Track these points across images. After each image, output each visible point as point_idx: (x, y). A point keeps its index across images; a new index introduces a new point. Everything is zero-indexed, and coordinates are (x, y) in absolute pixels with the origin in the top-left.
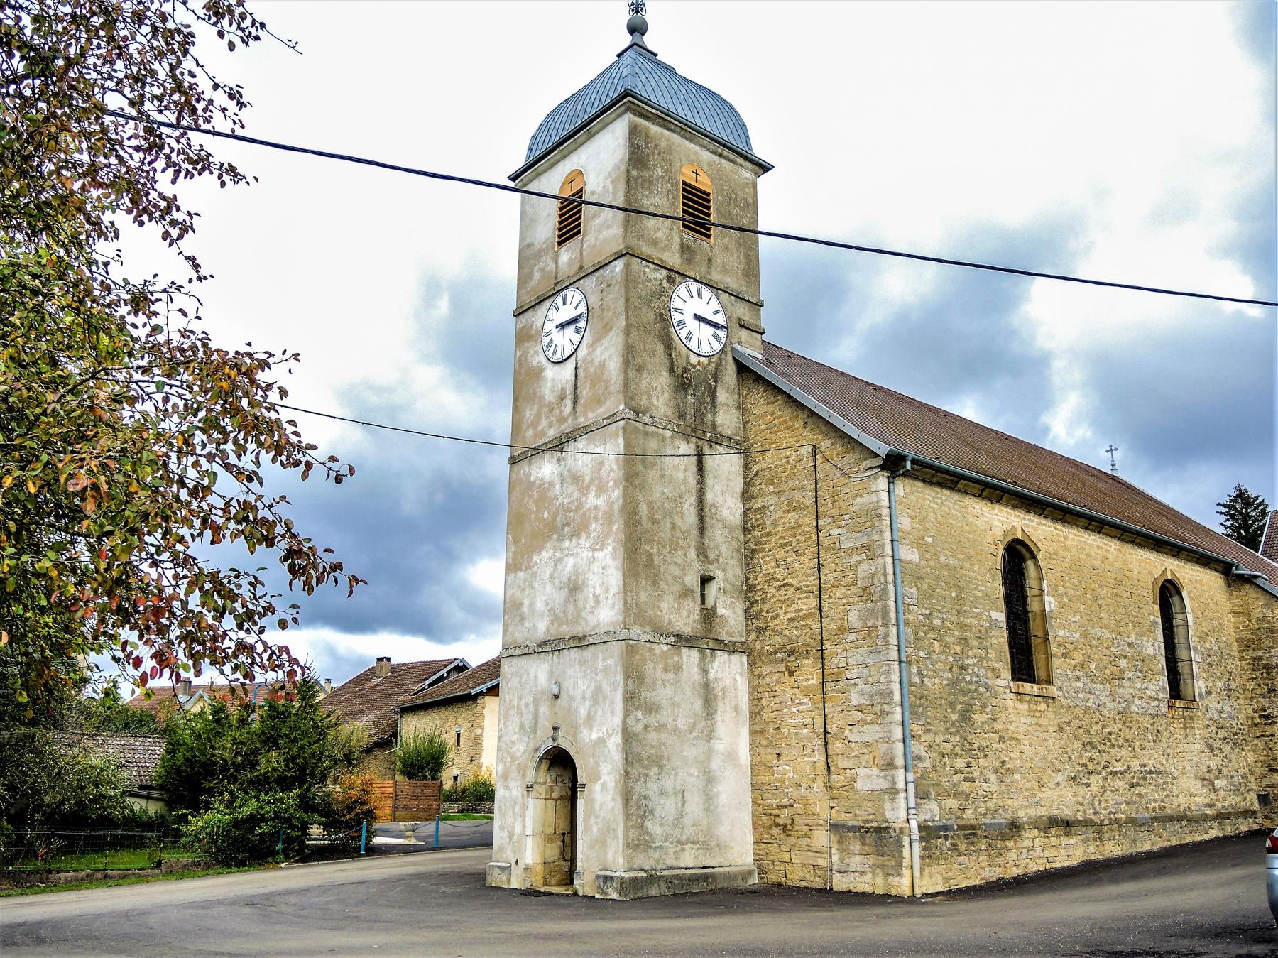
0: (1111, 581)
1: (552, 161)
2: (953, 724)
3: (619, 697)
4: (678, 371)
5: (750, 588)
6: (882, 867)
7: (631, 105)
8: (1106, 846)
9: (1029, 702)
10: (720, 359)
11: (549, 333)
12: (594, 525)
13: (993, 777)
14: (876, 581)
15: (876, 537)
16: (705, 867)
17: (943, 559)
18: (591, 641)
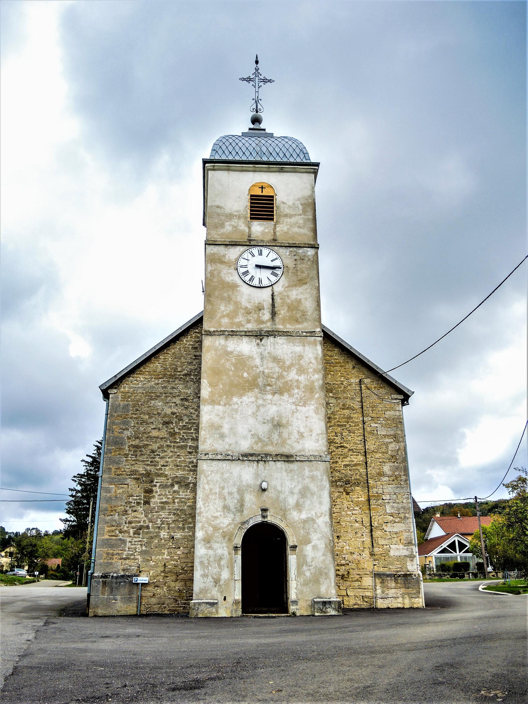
1: (244, 168)
6: (408, 594)
14: (399, 453)
18: (298, 459)
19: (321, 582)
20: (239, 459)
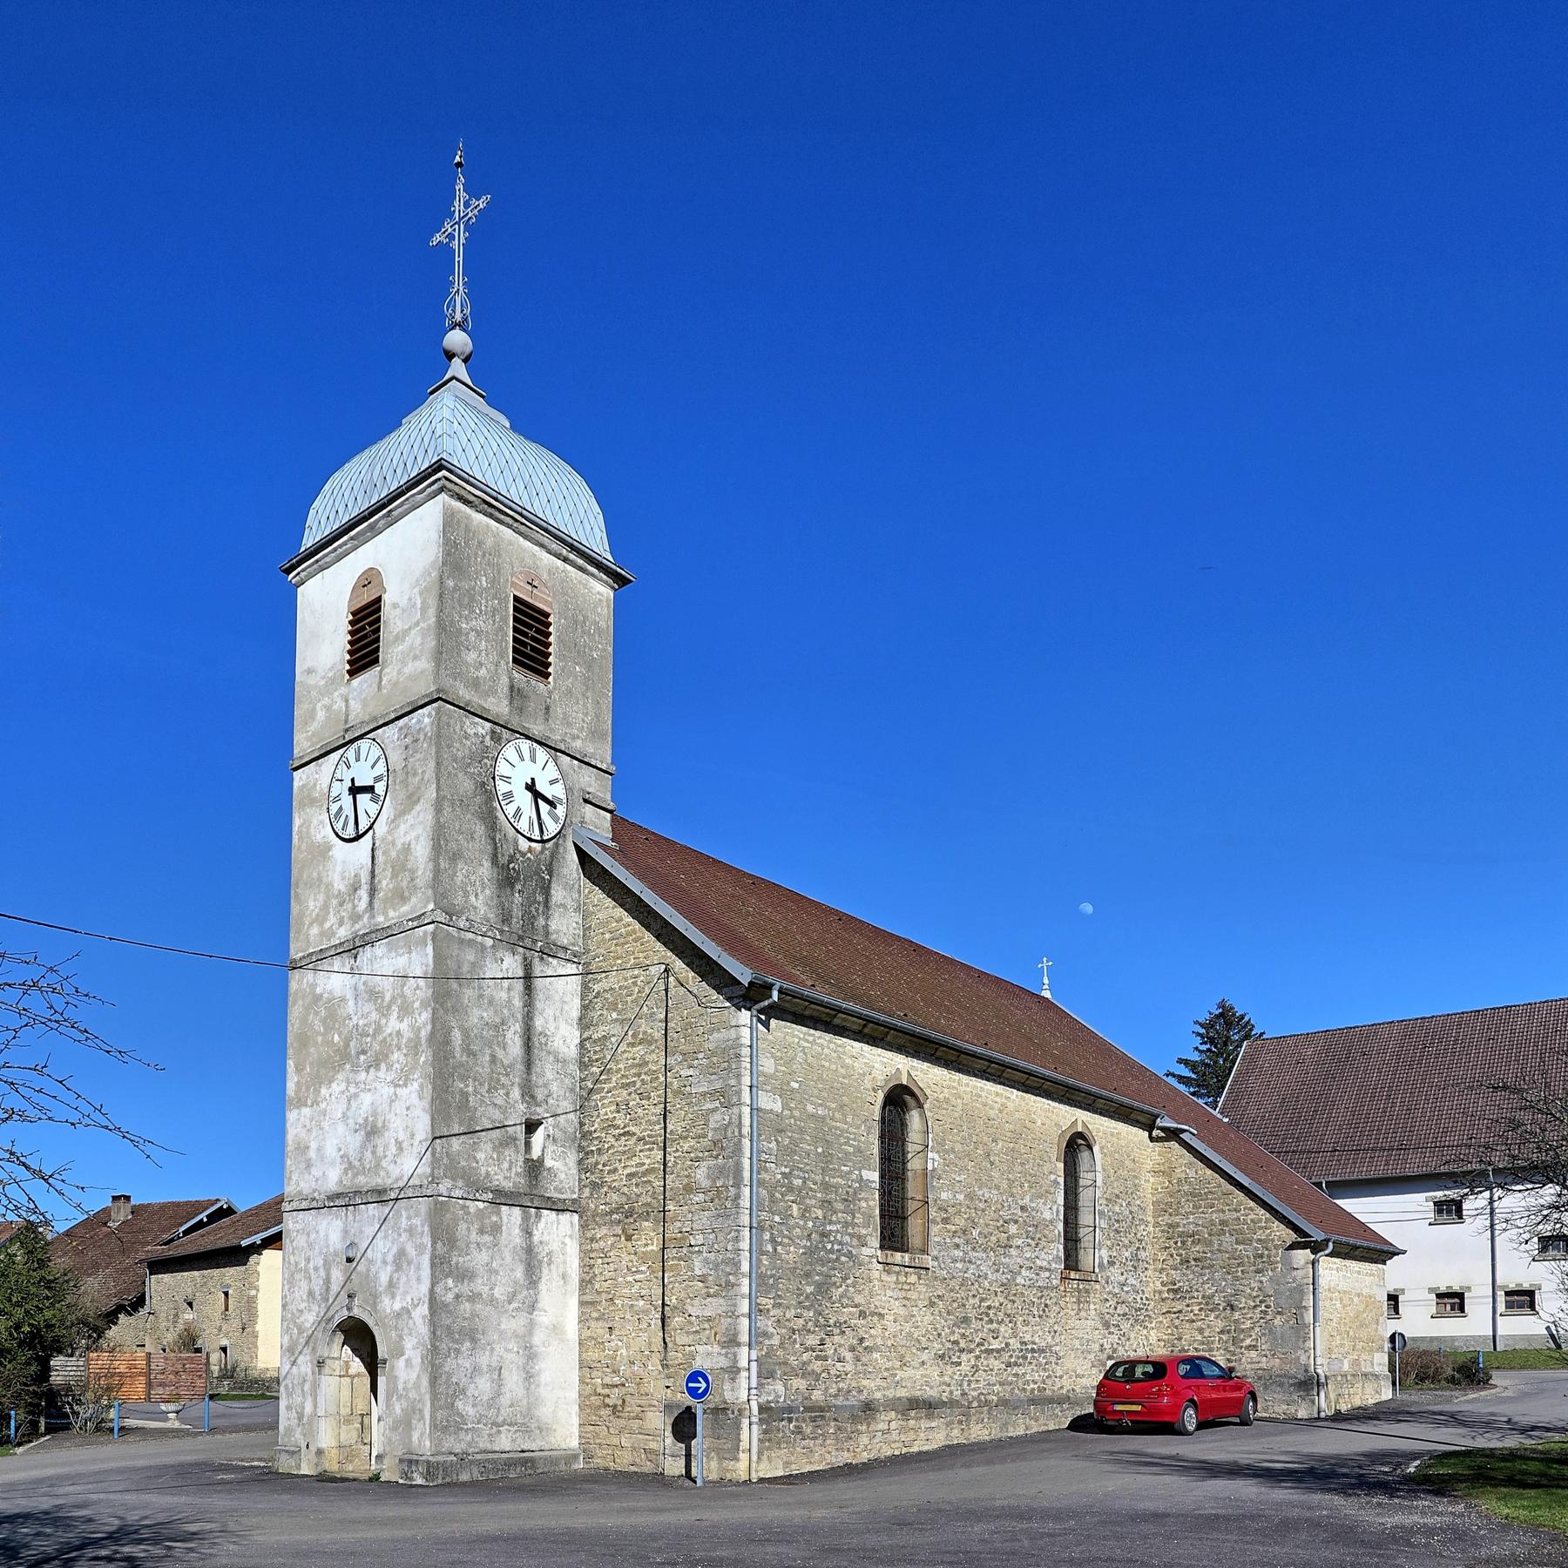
0: (1009, 1134)
2: (807, 1297)
3: (426, 1261)
4: (503, 860)
5: (584, 1136)
6: (718, 1451)
7: (447, 483)
8: (972, 1431)
9: (898, 1273)
10: (557, 845)
11: (337, 799)
12: (396, 1055)
13: (849, 1356)
15: (733, 1082)
16: (523, 1451)
17: (810, 1108)
19: (414, 1426)
20: (325, 1206)
